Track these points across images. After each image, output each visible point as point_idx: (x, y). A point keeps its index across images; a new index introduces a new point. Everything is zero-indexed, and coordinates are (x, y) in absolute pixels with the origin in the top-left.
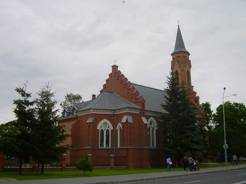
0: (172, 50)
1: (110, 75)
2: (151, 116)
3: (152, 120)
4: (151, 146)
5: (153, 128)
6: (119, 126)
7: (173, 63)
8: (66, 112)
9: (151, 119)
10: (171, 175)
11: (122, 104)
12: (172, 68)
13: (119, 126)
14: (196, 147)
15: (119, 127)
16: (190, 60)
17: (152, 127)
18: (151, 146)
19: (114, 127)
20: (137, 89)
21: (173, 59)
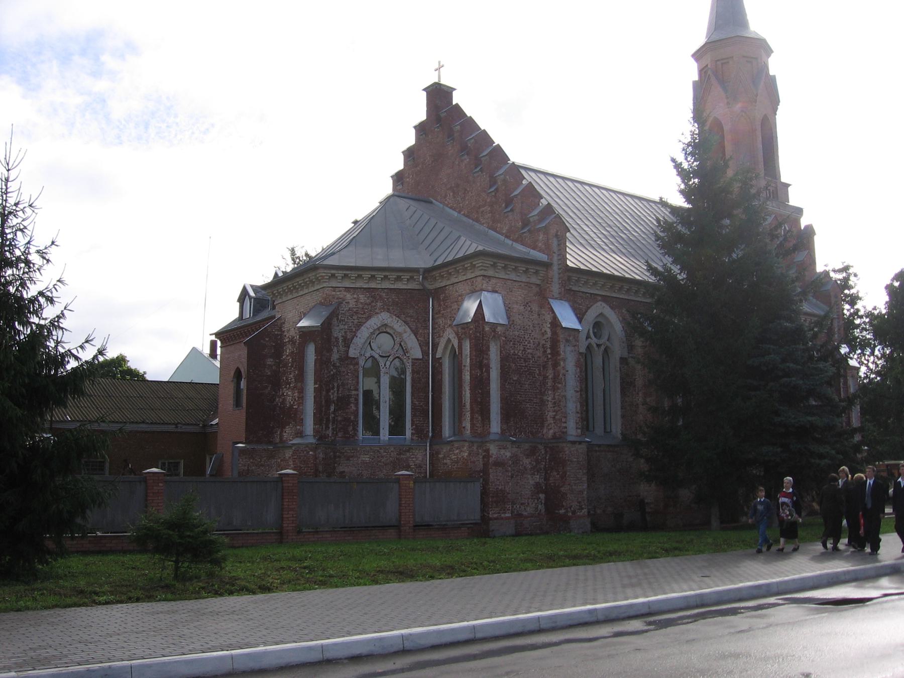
0: (699, 38)
1: (421, 129)
2: (594, 298)
3: (601, 314)
4: (599, 430)
5: (606, 351)
6: (449, 340)
7: (701, 91)
8: (249, 296)
9: (599, 308)
10: (538, 182)
11: (463, 239)
12: (698, 116)
13: (449, 340)
14: (168, 478)
15: (446, 348)
16: (771, 73)
17: (603, 348)
18: (599, 430)
19: (424, 345)
20: (549, 195)
21: (702, 72)
